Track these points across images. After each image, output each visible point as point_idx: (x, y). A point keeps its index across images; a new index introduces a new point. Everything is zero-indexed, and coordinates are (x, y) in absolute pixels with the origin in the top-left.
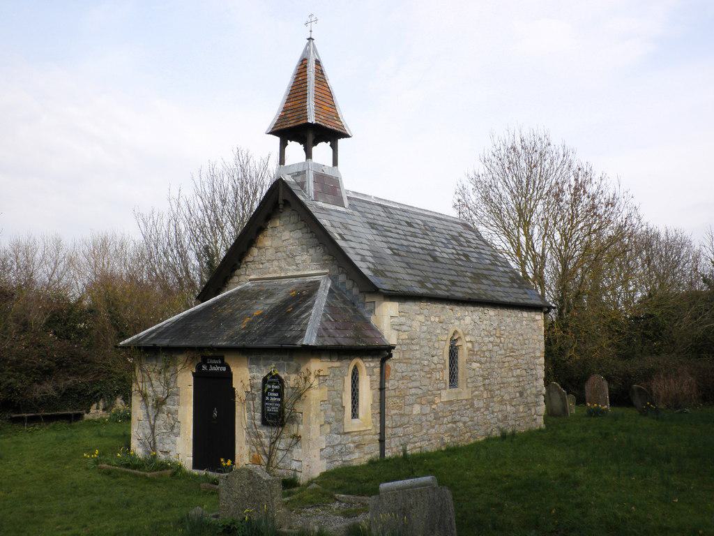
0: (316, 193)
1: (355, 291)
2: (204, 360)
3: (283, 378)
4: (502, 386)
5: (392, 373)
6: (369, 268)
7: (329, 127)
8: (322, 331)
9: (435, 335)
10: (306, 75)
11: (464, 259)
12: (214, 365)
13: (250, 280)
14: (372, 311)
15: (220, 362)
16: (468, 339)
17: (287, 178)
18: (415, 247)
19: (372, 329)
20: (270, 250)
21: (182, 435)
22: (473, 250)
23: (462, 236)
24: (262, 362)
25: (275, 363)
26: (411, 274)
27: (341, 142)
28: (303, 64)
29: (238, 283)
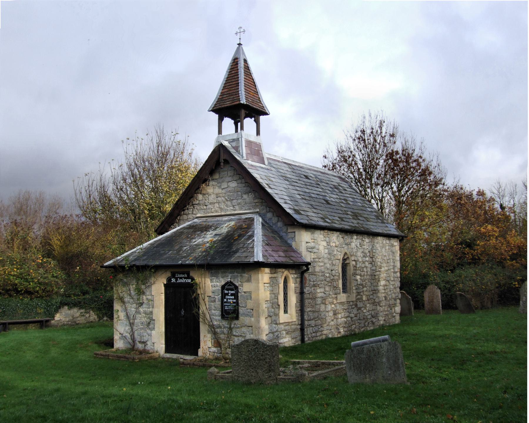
0: (247, 154)
1: (280, 224)
2: (173, 275)
3: (237, 285)
4: (374, 292)
5: (308, 282)
6: (290, 208)
7: (255, 107)
8: (264, 252)
9: (333, 256)
10: (238, 69)
11: (344, 202)
12: (181, 278)
13: (197, 218)
14: (293, 238)
15: (186, 276)
16: (353, 258)
17: (226, 143)
18: (314, 194)
19: (294, 251)
20: (212, 196)
21: (156, 329)
22: (348, 196)
23: (340, 186)
24: (220, 275)
25: (231, 275)
26: (315, 213)
27: (262, 118)
28: (235, 62)
29: (187, 220)
